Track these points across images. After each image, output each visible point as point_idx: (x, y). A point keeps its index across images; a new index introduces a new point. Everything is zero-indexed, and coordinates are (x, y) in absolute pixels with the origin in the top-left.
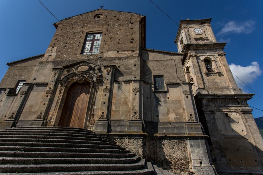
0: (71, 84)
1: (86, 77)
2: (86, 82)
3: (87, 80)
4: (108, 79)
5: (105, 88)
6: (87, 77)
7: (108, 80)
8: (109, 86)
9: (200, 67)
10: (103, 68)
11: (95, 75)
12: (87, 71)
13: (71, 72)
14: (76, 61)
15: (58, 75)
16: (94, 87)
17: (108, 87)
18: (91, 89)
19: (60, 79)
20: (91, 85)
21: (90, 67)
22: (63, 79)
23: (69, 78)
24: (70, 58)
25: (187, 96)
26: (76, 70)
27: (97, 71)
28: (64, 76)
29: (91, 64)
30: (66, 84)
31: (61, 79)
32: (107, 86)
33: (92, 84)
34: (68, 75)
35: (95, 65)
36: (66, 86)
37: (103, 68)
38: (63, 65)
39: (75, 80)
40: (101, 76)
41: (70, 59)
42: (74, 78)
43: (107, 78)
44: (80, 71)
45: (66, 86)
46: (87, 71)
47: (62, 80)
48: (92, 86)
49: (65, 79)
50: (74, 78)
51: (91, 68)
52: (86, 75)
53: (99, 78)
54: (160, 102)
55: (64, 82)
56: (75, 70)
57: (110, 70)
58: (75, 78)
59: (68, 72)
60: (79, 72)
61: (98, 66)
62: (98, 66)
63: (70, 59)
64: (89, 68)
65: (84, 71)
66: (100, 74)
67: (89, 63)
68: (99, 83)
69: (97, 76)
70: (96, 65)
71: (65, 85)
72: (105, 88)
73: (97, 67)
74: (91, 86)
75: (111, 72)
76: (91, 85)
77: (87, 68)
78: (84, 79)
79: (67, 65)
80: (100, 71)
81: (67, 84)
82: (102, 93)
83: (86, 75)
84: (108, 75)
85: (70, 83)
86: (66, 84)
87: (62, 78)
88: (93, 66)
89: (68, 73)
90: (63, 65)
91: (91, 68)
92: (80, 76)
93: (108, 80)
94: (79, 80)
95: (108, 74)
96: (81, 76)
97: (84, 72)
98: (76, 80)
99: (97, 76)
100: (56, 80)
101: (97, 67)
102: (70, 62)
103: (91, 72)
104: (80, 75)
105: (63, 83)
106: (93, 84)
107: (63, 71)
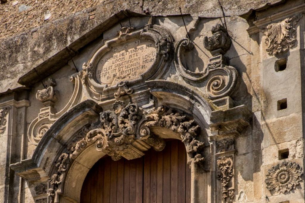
0: (86, 171)
1: (155, 115)
2: (159, 147)
3: (164, 133)
4: (281, 97)
5: (277, 161)
6: (160, 114)
7: (283, 105)
8: (299, 149)
9: (187, 73)
10: (240, 31)
11: (203, 91)
12: (151, 84)
13: (66, 107)
14: (83, 26)
15: (9, 136)
16: (207, 171)
17: (291, 153)
18: (196, 182)
19: (25, 157)
20: (189, 159)
21: (162, 48)
22: (38, 153)
23: (66, 137)
24: (46, 10)
25: (274, 105)
26: (92, 81)
27: (206, 57)
28: (39, 137)
29: (168, 25)
30: (57, 179)
31: (30, 156)
32: (283, 146)
33: (193, 154)
34: (58, 126)
35: (191, 25)
36: (59, 191)
37: (240, 31)
38: (21, 66)
39: (98, 150)
40: (238, 92)
41: (47, 16)
42: (91, 136)
43: (277, 95)
44: (114, 86)
45: (59, 191)
46: (154, 71)
47: (33, 164)
48: (198, 165)
49: (45, 151)
50: (91, 136)
51: (171, 53)
52: (151, 103)
53: (225, 107)
54: (158, 115)
55: (48, 169)
56: (87, 83)
57: (292, 32)
58: (95, 134)
59: (54, 103)
60: (110, 92)
61: (212, 24)
62: (212, 24)
63: (47, 16)
64: (159, 55)
65: (138, 77)
66: (227, 78)
67: (156, 20)
68: (237, 136)
69: (212, 93)
70: (201, 21)
71: (56, 186)
72: (277, 161)
73: (207, 31)
74: (193, 167)
75: (294, 44)
76: (192, 162)
77: (144, 56)
78: (143, 132)
79: (41, 61)
80: (229, 54)
81: (62, 177)
82: (263, 197)
83: (151, 103)
84: (280, 73)
85: (76, 166)
86: (57, 179)
87: (32, 145)
88: (180, 33)
89: (54, 111)
90: (21, 66)
91: (171, 53)
92: (120, 119)
93: (283, 105)
94: (120, 144)
95: (281, 67)
96: (125, 117)
97: (138, 82)
98: (100, 146)
99: (212, 93)
100: (7, 165)
101: (207, 31)
102: (49, 39)
103: (177, 76)
104: (120, 110)
105: (42, 174)
106: (202, 150)
107: (26, 107)
